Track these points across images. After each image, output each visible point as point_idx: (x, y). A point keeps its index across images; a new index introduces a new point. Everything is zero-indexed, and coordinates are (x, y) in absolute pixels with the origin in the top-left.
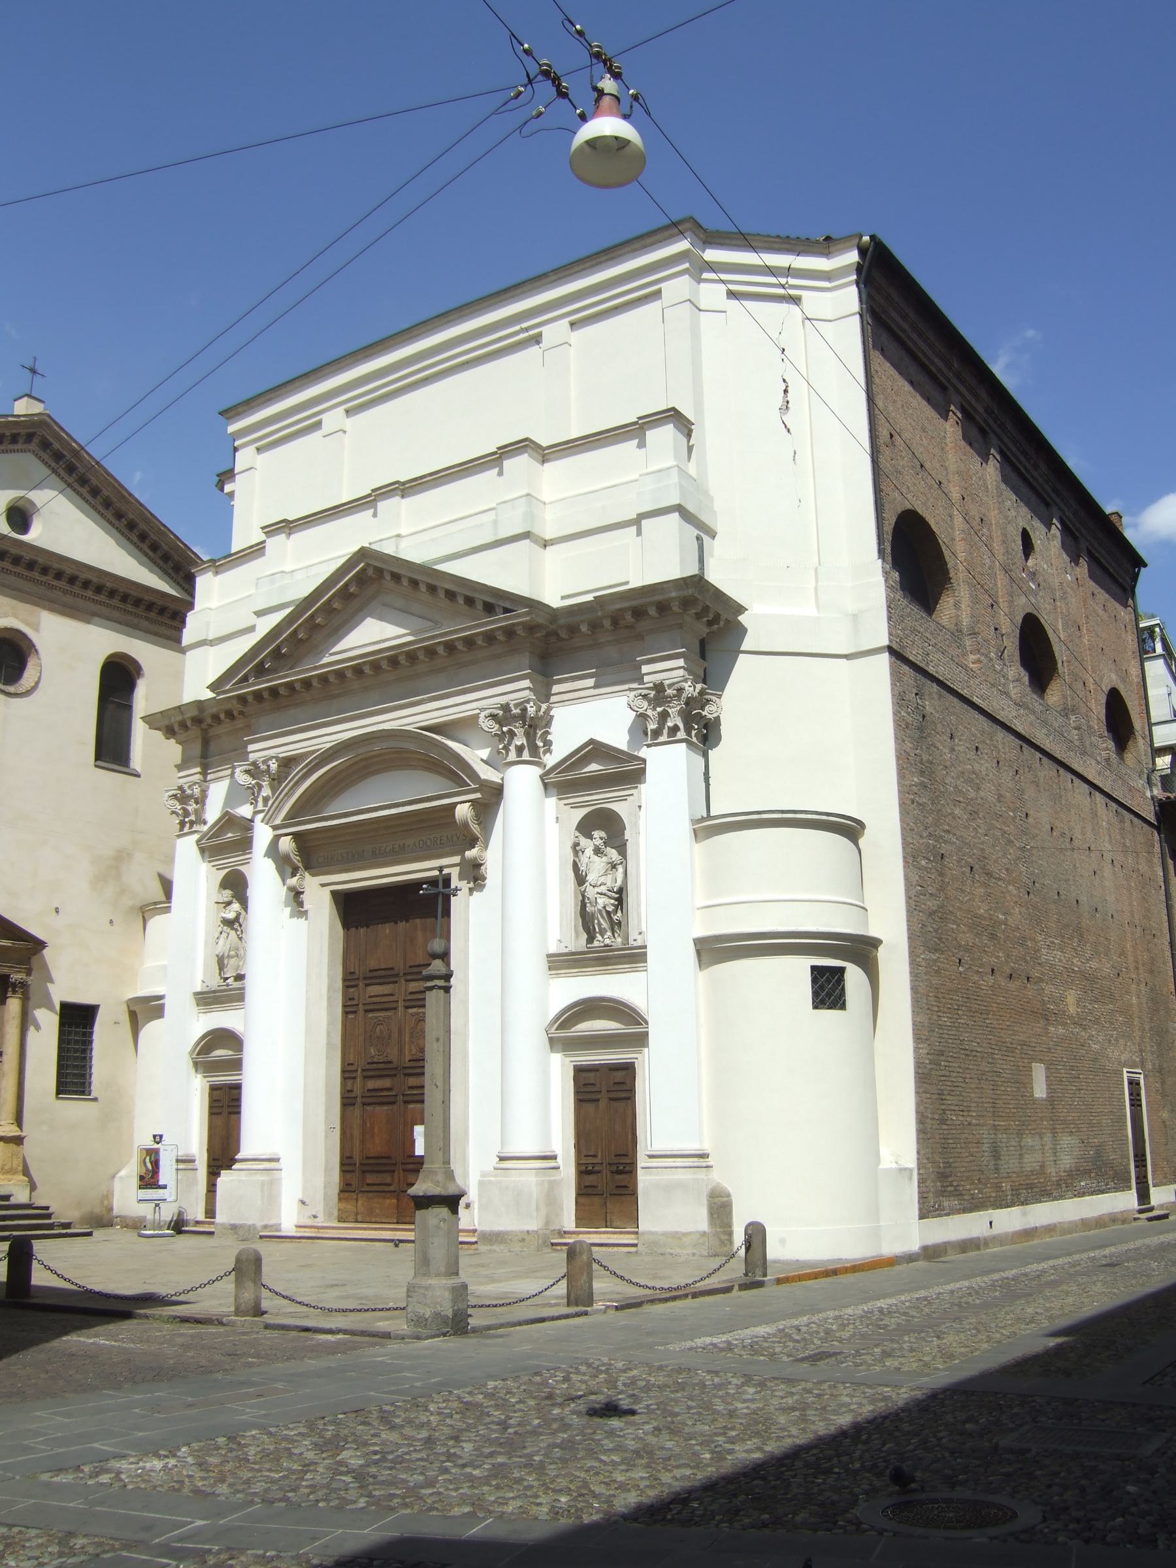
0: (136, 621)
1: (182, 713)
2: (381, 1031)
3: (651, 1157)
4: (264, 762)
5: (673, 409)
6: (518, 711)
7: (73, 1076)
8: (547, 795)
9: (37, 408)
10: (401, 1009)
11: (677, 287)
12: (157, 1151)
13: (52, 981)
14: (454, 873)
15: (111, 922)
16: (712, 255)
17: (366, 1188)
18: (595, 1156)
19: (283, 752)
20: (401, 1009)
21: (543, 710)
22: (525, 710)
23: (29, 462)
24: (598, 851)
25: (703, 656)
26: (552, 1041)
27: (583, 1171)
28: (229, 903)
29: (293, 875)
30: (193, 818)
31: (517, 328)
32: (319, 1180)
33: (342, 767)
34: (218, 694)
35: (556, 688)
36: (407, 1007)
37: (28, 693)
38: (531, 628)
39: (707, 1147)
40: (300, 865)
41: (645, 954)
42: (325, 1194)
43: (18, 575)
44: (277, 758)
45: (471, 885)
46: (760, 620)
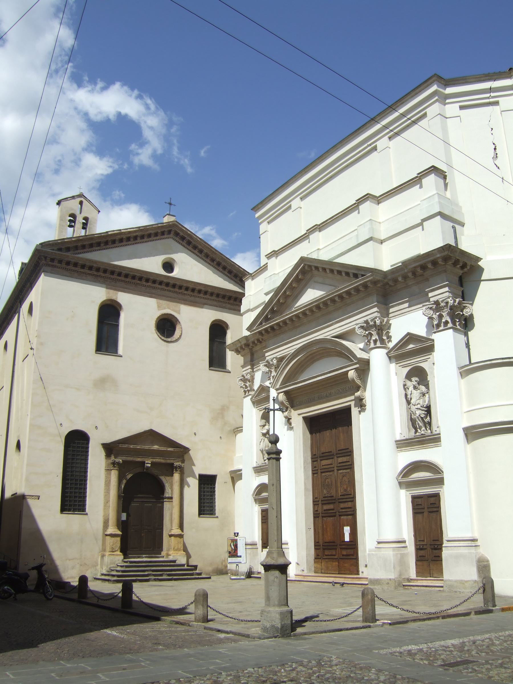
0: (224, 305)
1: (240, 343)
2: (328, 482)
3: (448, 541)
4: (272, 360)
5: (433, 166)
6: (373, 323)
7: (207, 506)
8: (391, 362)
9: (172, 219)
10: (336, 471)
11: (434, 109)
12: (236, 540)
13: (194, 465)
14: (352, 404)
15: (221, 437)
16: (450, 90)
17: (325, 557)
18: (423, 541)
19: (279, 355)
20: (336, 471)
21: (385, 321)
22: (375, 322)
23: (170, 242)
24: (415, 388)
25: (461, 285)
27: (419, 549)
28: (264, 426)
29: (286, 411)
30: (249, 389)
31: (366, 145)
32: (304, 553)
33: (302, 359)
34: (251, 332)
35: (391, 310)
36: (338, 470)
37: (177, 340)
38: (375, 283)
39: (476, 535)
40: (289, 406)
41: (440, 438)
42: (307, 560)
44: (276, 358)
45: (360, 409)
46: (490, 263)
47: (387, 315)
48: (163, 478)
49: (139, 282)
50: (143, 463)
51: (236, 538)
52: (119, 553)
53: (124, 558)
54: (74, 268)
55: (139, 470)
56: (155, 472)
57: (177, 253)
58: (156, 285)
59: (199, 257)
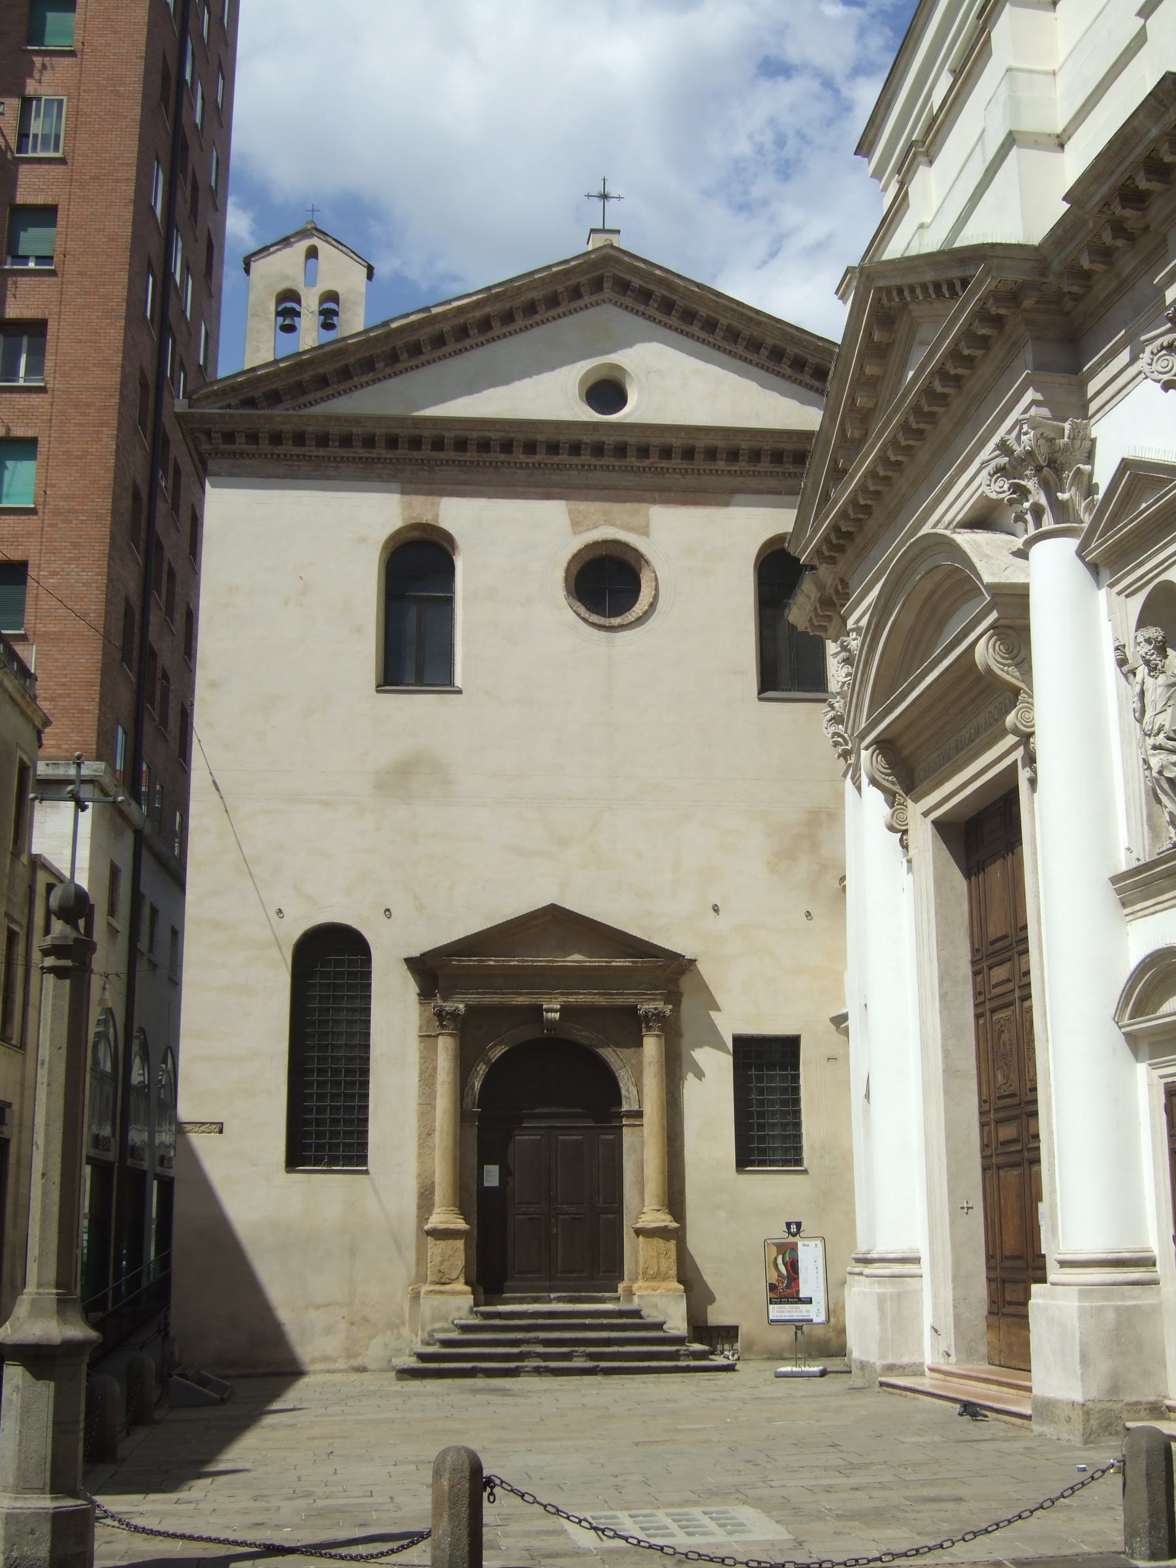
3: (1064, 1264)
12: (793, 1248)
13: (718, 1009)
15: (808, 914)
23: (608, 315)
26: (1132, 1039)
35: (1093, 387)
38: (1012, 296)
40: (897, 788)
43: (607, 468)
47: (1082, 409)
48: (609, 1054)
49: (503, 457)
50: (539, 1009)
51: (791, 1239)
52: (460, 1286)
53: (476, 1304)
54: (296, 450)
55: (527, 1033)
56: (581, 1034)
57: (629, 344)
58: (563, 458)
59: (709, 344)
